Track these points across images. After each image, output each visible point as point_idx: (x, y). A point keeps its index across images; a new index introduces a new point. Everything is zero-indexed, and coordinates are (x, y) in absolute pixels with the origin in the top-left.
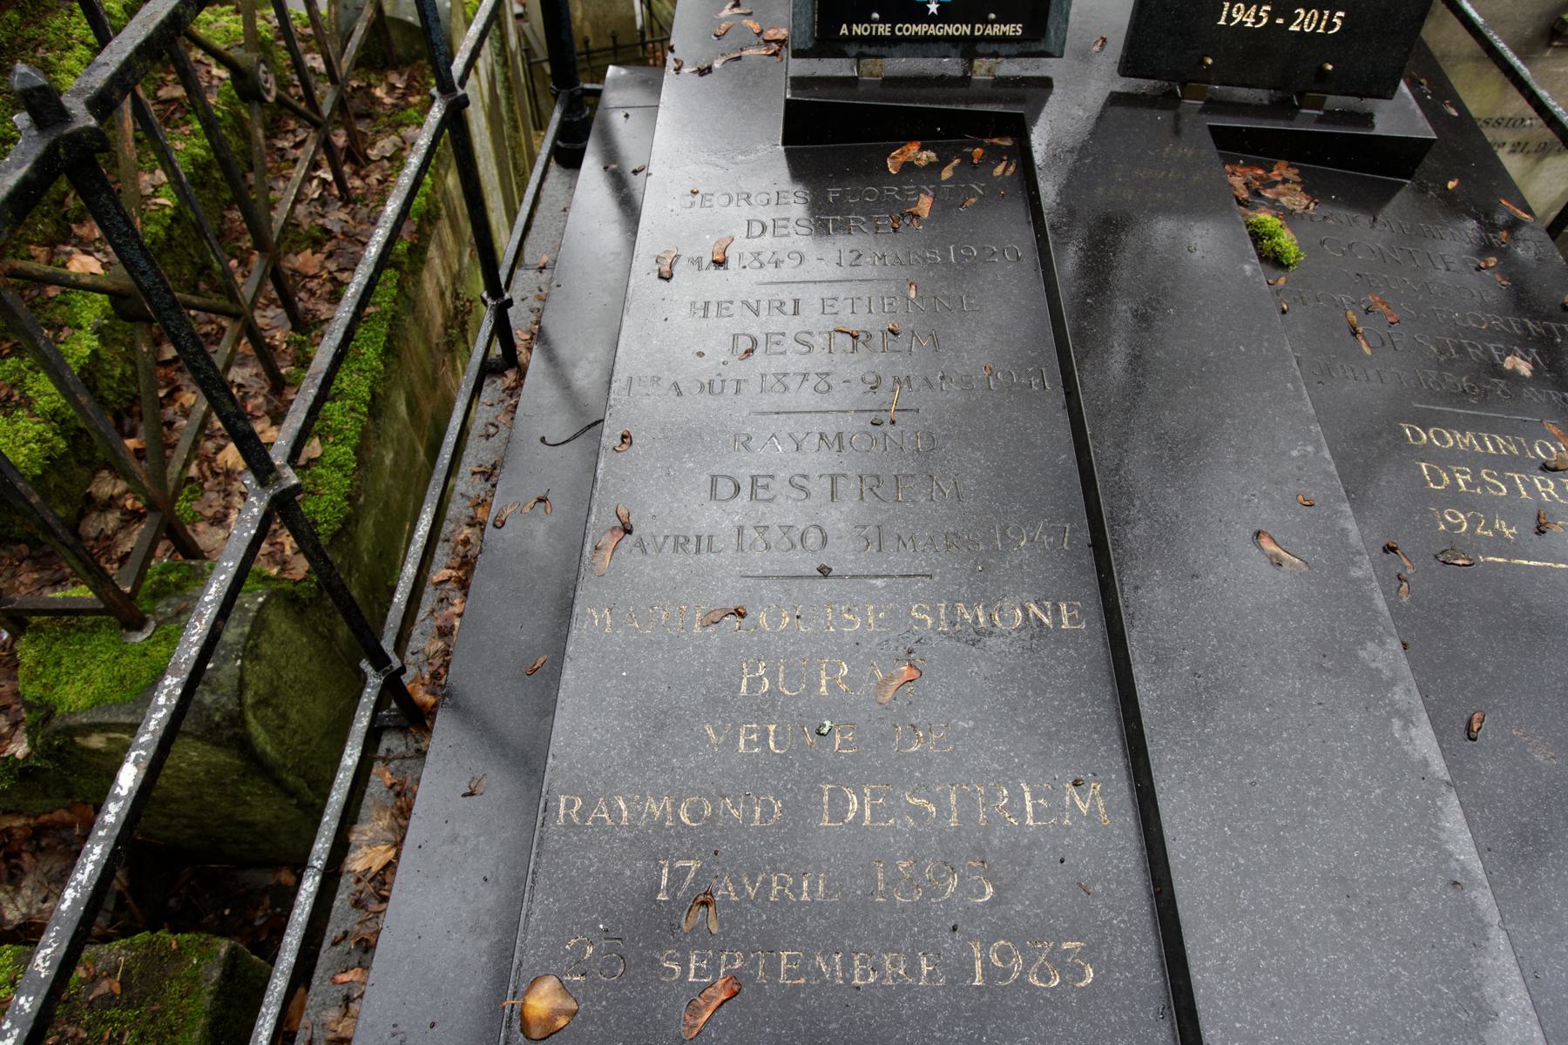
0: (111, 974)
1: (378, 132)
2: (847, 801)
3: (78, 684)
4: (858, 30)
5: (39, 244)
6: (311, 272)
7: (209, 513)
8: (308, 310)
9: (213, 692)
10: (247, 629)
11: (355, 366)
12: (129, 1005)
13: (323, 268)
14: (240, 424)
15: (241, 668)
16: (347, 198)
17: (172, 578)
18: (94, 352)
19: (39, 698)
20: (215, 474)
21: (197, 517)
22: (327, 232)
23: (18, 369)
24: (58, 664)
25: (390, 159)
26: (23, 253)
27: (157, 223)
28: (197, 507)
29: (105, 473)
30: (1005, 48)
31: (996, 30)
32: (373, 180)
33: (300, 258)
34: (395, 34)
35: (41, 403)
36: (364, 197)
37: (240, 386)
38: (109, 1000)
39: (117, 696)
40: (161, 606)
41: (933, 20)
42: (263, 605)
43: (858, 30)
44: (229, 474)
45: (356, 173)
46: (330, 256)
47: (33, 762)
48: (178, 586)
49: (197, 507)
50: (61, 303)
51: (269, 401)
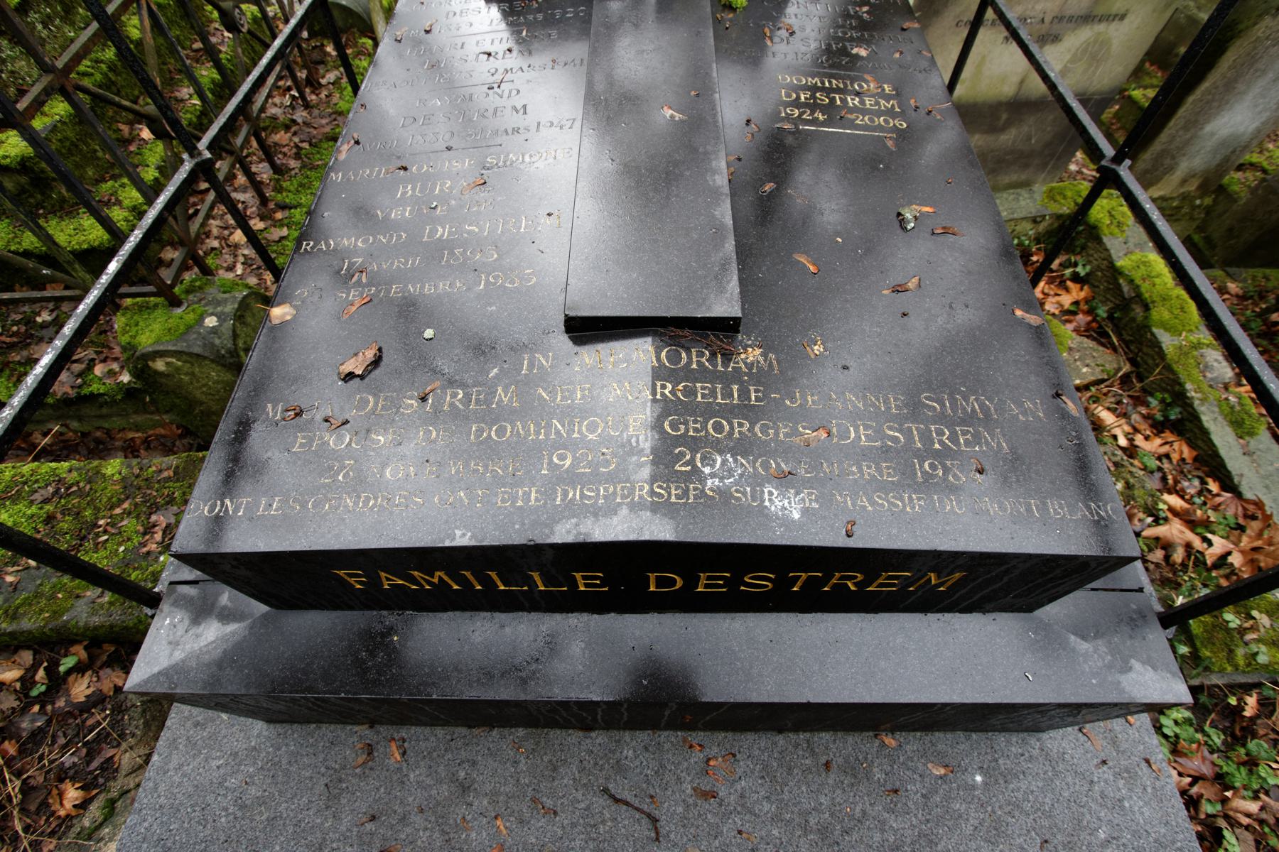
0: (168, 469)
1: (328, 71)
2: (437, 231)
3: (148, 334)
5: (123, 123)
6: (284, 143)
7: (225, 265)
8: (283, 164)
9: (219, 338)
10: (236, 306)
11: (309, 191)
12: (178, 481)
13: (291, 140)
14: (169, 113)
15: (234, 325)
16: (307, 106)
17: (198, 284)
19: (129, 343)
20: (229, 246)
21: (218, 267)
22: (294, 121)
23: (114, 186)
24: (137, 325)
25: (333, 84)
26: (114, 127)
27: (191, 113)
28: (218, 262)
29: (169, 248)
32: (323, 96)
33: (278, 136)
34: (336, 13)
35: (126, 203)
36: (318, 105)
37: (243, 202)
38: (168, 479)
39: (168, 338)
40: (191, 297)
42: (245, 297)
44: (236, 246)
45: (313, 92)
46: (295, 134)
47: (133, 385)
48: (200, 288)
49: (218, 262)
50: (137, 154)
51: (259, 209)
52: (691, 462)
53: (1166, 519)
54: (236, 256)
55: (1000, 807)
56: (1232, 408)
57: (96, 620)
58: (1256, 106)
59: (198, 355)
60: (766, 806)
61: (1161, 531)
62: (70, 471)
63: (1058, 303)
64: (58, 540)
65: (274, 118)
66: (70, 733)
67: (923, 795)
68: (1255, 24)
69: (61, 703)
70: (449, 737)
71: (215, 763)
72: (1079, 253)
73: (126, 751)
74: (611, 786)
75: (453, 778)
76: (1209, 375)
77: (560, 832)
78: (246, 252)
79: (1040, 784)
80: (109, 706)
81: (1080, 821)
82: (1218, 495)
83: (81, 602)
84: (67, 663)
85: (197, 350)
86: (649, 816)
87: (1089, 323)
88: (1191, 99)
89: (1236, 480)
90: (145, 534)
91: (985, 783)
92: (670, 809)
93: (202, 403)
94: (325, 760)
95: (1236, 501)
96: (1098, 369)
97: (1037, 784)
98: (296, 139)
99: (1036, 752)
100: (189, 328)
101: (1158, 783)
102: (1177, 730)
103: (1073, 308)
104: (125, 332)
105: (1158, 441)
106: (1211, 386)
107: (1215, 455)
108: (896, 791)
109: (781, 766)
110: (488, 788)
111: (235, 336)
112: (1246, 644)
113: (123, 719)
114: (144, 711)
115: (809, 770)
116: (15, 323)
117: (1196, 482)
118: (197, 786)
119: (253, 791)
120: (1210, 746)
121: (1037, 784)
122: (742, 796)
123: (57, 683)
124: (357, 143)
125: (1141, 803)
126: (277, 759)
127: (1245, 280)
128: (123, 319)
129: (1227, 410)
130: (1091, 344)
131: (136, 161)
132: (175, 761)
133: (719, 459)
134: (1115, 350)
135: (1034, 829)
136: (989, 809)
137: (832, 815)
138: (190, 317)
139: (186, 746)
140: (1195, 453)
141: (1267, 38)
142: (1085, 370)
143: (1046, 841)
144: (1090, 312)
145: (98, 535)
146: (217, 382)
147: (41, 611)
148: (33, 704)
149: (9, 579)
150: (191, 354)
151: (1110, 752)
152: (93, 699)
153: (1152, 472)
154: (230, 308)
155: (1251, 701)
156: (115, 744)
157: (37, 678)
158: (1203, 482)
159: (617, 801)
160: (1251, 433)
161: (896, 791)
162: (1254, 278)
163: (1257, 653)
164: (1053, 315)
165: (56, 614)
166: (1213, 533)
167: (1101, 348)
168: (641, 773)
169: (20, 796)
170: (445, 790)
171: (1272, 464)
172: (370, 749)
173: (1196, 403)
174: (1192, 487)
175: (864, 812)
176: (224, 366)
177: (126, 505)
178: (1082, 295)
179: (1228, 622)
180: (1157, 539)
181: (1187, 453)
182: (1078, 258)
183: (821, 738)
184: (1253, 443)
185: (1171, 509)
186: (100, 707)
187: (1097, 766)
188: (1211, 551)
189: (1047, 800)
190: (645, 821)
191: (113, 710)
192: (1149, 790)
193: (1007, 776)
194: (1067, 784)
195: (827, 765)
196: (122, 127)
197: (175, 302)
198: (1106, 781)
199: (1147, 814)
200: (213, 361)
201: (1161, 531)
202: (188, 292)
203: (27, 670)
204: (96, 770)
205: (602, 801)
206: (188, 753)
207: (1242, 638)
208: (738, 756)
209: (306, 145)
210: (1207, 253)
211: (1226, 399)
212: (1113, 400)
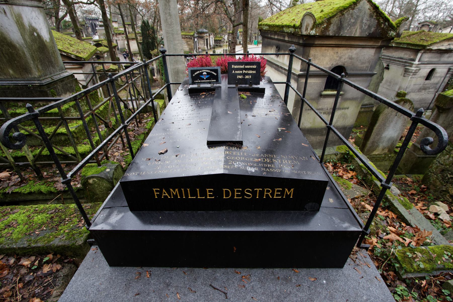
4: (197, 81)
12: (91, 209)
16: (138, 127)
18: (98, 139)
22: (135, 130)
30: (214, 83)
31: (213, 81)
32: (142, 125)
34: (148, 108)
38: (89, 208)
40: (103, 165)
41: (205, 80)
43: (197, 81)
46: (134, 132)
52: (232, 163)
53: (390, 233)
54: (114, 158)
55: (332, 290)
56: (402, 201)
57: (60, 244)
58: (394, 130)
59: (103, 178)
60: (260, 290)
61: (389, 236)
62: (60, 206)
63: (347, 176)
64: (53, 223)
65: (129, 129)
66: (40, 283)
67: (308, 287)
68: (384, 110)
69: (39, 273)
70: (164, 271)
71: (92, 279)
72: (350, 163)
73: (55, 290)
74: (213, 284)
75: (165, 282)
76: (393, 192)
77: (196, 298)
78: (117, 157)
79: (344, 283)
80: (53, 276)
81: (357, 294)
82: (405, 227)
83: (57, 239)
84: (46, 259)
85: (103, 176)
86: (224, 293)
87: (357, 181)
88: (375, 128)
89: (409, 222)
90: (79, 222)
91: (326, 283)
92: (231, 291)
93: (97, 194)
94: (126, 277)
95: (411, 228)
96: (362, 193)
97: (342, 284)
98: (134, 133)
99: (341, 274)
100: (102, 171)
101: (380, 284)
102: (402, 293)
103: (352, 177)
104: (84, 172)
105: (384, 212)
106: (394, 195)
107: (402, 215)
108: (299, 285)
109: (264, 278)
110: (175, 285)
111: (114, 174)
112: (416, 262)
113: (56, 280)
114: (63, 279)
115: (273, 279)
116: (50, 173)
117: (398, 223)
118: (85, 285)
119: (103, 286)
120: (414, 298)
121: (342, 284)
122: (253, 287)
123: (40, 267)
124: (163, 119)
125: (375, 289)
126: (111, 277)
127: (412, 178)
128: (84, 169)
129: (401, 202)
130: (358, 186)
131: (94, 135)
132: (79, 278)
133: (238, 163)
134: (365, 187)
135: (343, 296)
136: (329, 290)
137: (280, 293)
138: (103, 169)
139: (83, 274)
140: (396, 216)
141: (389, 113)
142: (358, 193)
143: (348, 300)
144: (357, 178)
145: (65, 222)
146: (105, 187)
147: (45, 241)
148: (31, 272)
149: (37, 233)
150: (101, 178)
151: (363, 274)
152: (49, 273)
153: (383, 221)
154: (114, 167)
155: (424, 282)
156: (52, 287)
157: (35, 264)
158: (400, 223)
159: (215, 288)
160: (410, 208)
161: (299, 285)
162: (415, 177)
163: (419, 265)
164: (346, 179)
165: (49, 242)
166: (406, 237)
167: (361, 187)
168: (222, 281)
169: (21, 299)
170: (162, 286)
171: (419, 217)
172: (140, 274)
173: (391, 200)
174: (397, 224)
175: (290, 291)
176: (109, 182)
177: (75, 215)
178: (354, 174)
179: (408, 255)
180: (388, 239)
181: (394, 216)
182: (350, 164)
183: (276, 271)
184: (411, 211)
185: (391, 230)
186: (50, 276)
187: (360, 278)
188: (406, 242)
189: (346, 288)
190: (223, 294)
191: (53, 278)
192: (378, 285)
193: (333, 281)
194: (352, 283)
195: (278, 278)
196: (92, 128)
197: (99, 165)
198: (363, 282)
199: (378, 292)
200: (106, 180)
201: (389, 236)
202: (103, 163)
203: (32, 262)
204: (45, 295)
205: (210, 289)
206: (84, 276)
207: (414, 260)
208: (251, 276)
209: (137, 135)
210: (400, 171)
211: (400, 199)
212: (368, 201)
